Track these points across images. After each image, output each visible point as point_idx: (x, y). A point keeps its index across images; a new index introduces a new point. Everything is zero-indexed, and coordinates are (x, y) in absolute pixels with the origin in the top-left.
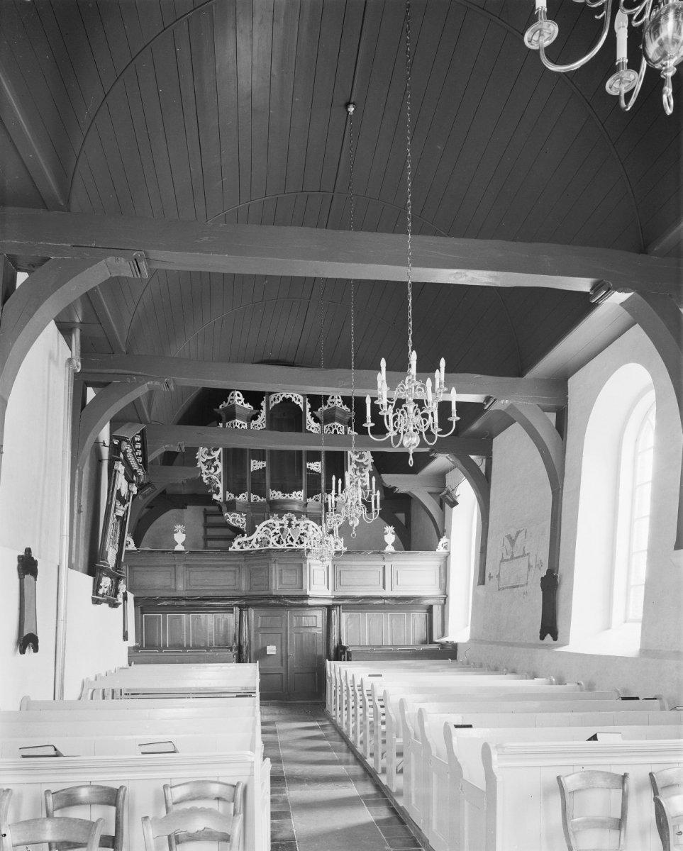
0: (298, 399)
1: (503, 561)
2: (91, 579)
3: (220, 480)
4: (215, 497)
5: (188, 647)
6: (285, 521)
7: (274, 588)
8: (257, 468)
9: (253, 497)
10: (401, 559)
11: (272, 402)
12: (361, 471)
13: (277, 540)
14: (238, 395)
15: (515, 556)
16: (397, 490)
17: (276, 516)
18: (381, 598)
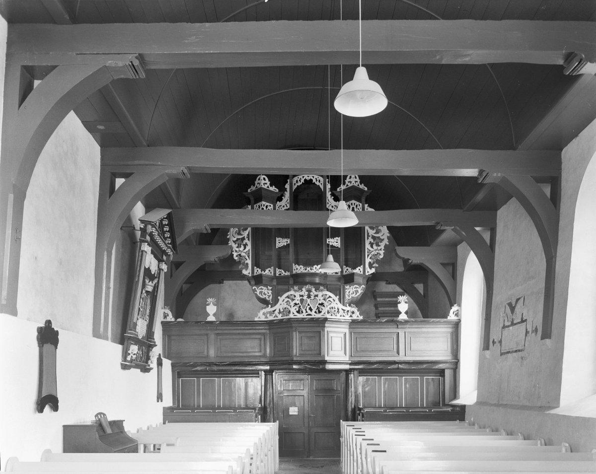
0: (319, 181)
1: (504, 327)
2: (120, 347)
4: (245, 272)
5: (219, 408)
6: (304, 292)
8: (281, 245)
9: (278, 271)
11: (295, 184)
12: (378, 245)
13: (297, 310)
14: (264, 179)
15: (515, 322)
16: (410, 261)
17: (296, 288)
18: (394, 363)
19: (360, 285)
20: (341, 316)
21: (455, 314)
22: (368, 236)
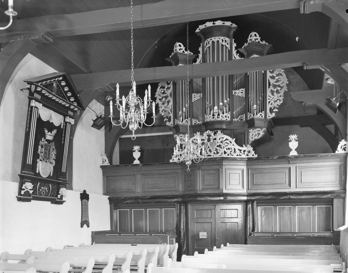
3: (171, 111)
7: (198, 188)
8: (196, 99)
9: (194, 121)
10: (304, 161)
12: (278, 92)
18: (285, 194)
19: (261, 128)
20: (237, 155)
21: (342, 148)
22: (269, 85)
